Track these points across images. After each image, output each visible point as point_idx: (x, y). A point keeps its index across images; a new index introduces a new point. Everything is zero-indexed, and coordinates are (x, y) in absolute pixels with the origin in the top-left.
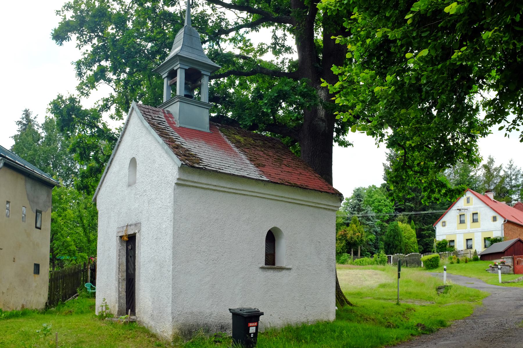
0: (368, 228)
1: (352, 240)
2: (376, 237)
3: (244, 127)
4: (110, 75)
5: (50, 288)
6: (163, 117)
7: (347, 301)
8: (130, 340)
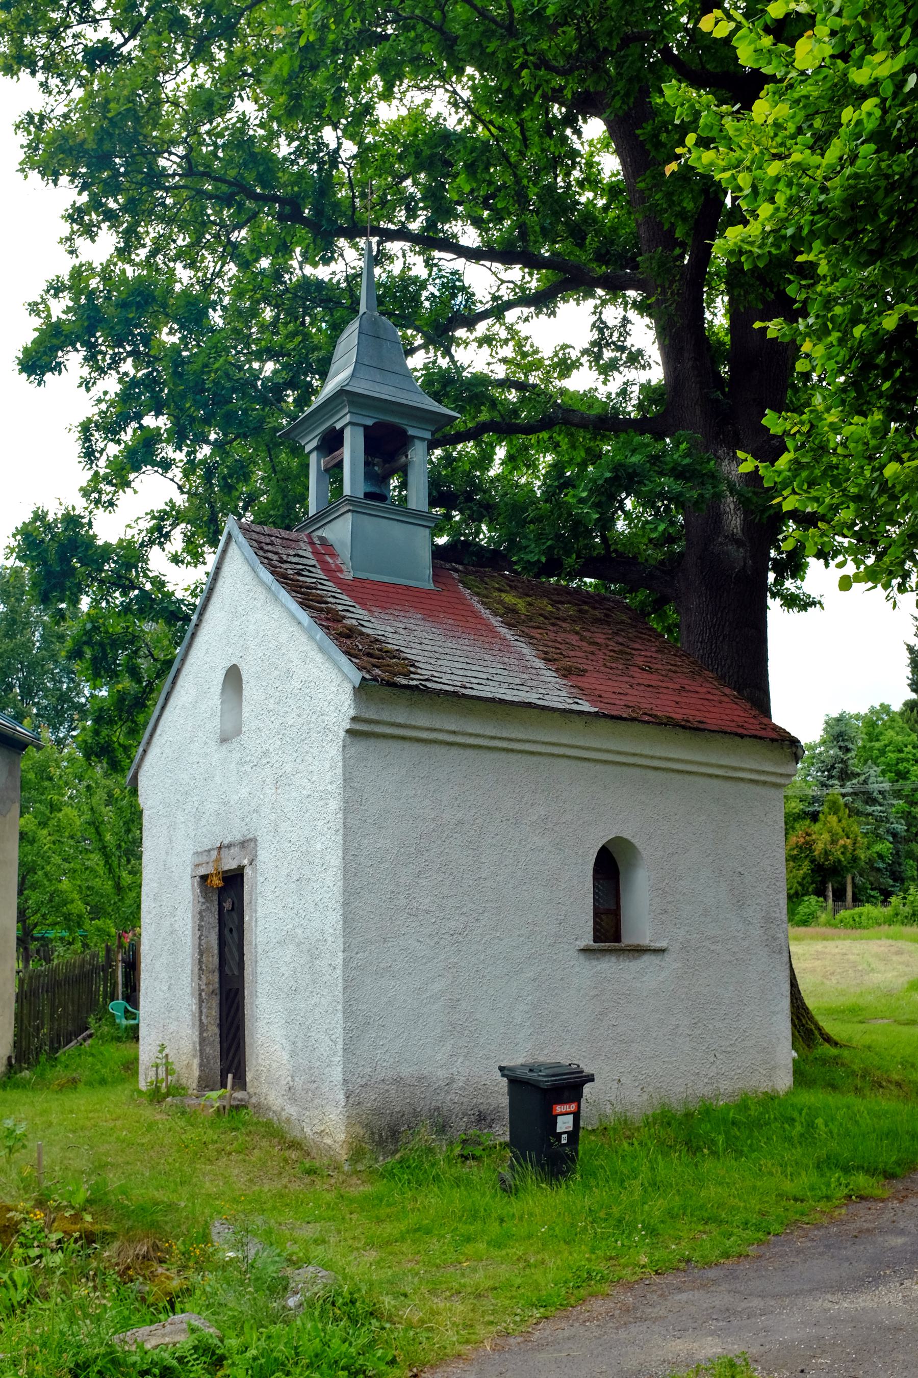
0: (872, 824)
1: (827, 860)
2: (895, 848)
3: (524, 568)
4: (168, 451)
5: (19, 1018)
6: (310, 556)
7: (821, 1034)
8: (232, 1158)
